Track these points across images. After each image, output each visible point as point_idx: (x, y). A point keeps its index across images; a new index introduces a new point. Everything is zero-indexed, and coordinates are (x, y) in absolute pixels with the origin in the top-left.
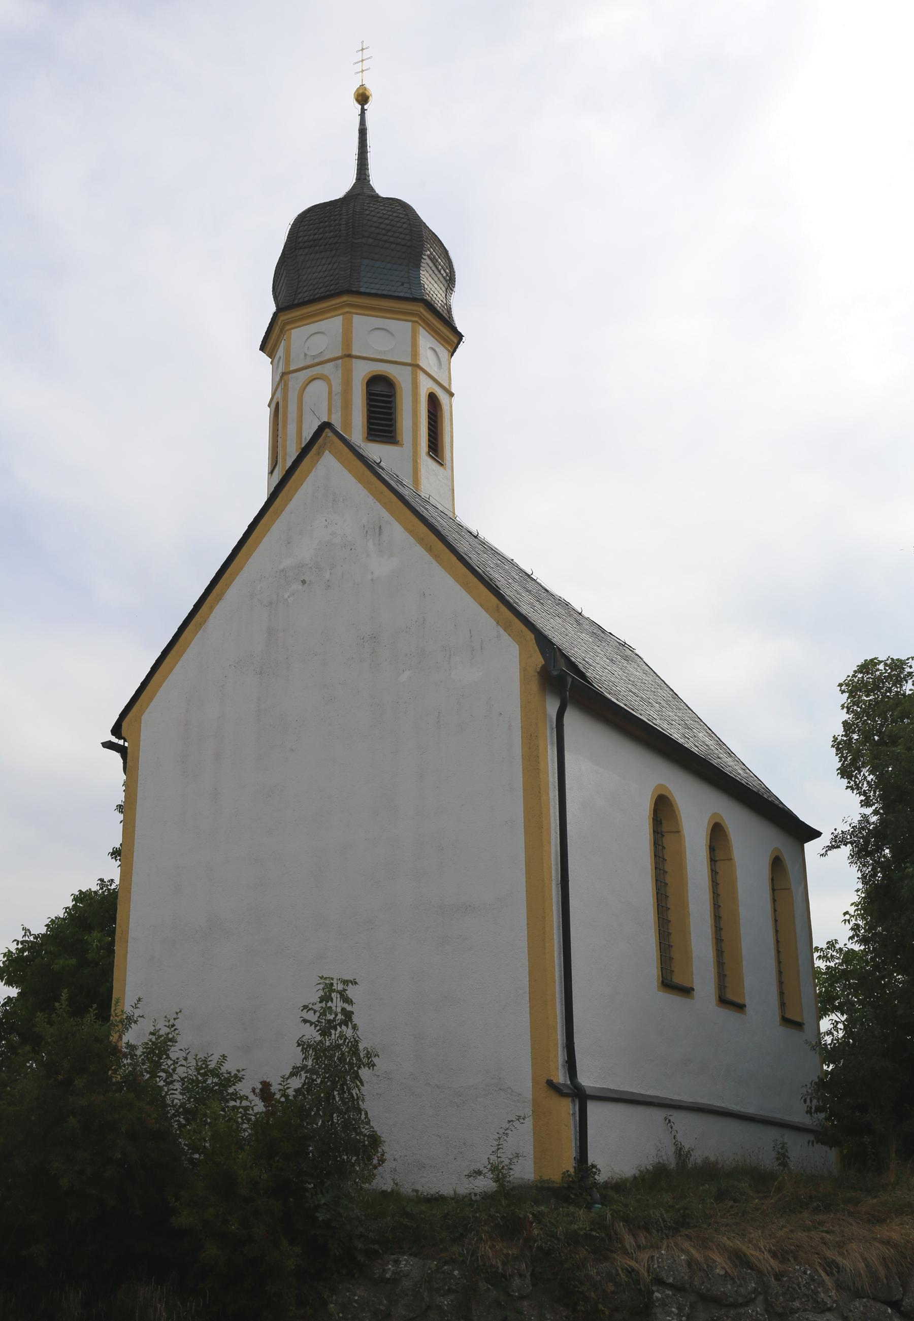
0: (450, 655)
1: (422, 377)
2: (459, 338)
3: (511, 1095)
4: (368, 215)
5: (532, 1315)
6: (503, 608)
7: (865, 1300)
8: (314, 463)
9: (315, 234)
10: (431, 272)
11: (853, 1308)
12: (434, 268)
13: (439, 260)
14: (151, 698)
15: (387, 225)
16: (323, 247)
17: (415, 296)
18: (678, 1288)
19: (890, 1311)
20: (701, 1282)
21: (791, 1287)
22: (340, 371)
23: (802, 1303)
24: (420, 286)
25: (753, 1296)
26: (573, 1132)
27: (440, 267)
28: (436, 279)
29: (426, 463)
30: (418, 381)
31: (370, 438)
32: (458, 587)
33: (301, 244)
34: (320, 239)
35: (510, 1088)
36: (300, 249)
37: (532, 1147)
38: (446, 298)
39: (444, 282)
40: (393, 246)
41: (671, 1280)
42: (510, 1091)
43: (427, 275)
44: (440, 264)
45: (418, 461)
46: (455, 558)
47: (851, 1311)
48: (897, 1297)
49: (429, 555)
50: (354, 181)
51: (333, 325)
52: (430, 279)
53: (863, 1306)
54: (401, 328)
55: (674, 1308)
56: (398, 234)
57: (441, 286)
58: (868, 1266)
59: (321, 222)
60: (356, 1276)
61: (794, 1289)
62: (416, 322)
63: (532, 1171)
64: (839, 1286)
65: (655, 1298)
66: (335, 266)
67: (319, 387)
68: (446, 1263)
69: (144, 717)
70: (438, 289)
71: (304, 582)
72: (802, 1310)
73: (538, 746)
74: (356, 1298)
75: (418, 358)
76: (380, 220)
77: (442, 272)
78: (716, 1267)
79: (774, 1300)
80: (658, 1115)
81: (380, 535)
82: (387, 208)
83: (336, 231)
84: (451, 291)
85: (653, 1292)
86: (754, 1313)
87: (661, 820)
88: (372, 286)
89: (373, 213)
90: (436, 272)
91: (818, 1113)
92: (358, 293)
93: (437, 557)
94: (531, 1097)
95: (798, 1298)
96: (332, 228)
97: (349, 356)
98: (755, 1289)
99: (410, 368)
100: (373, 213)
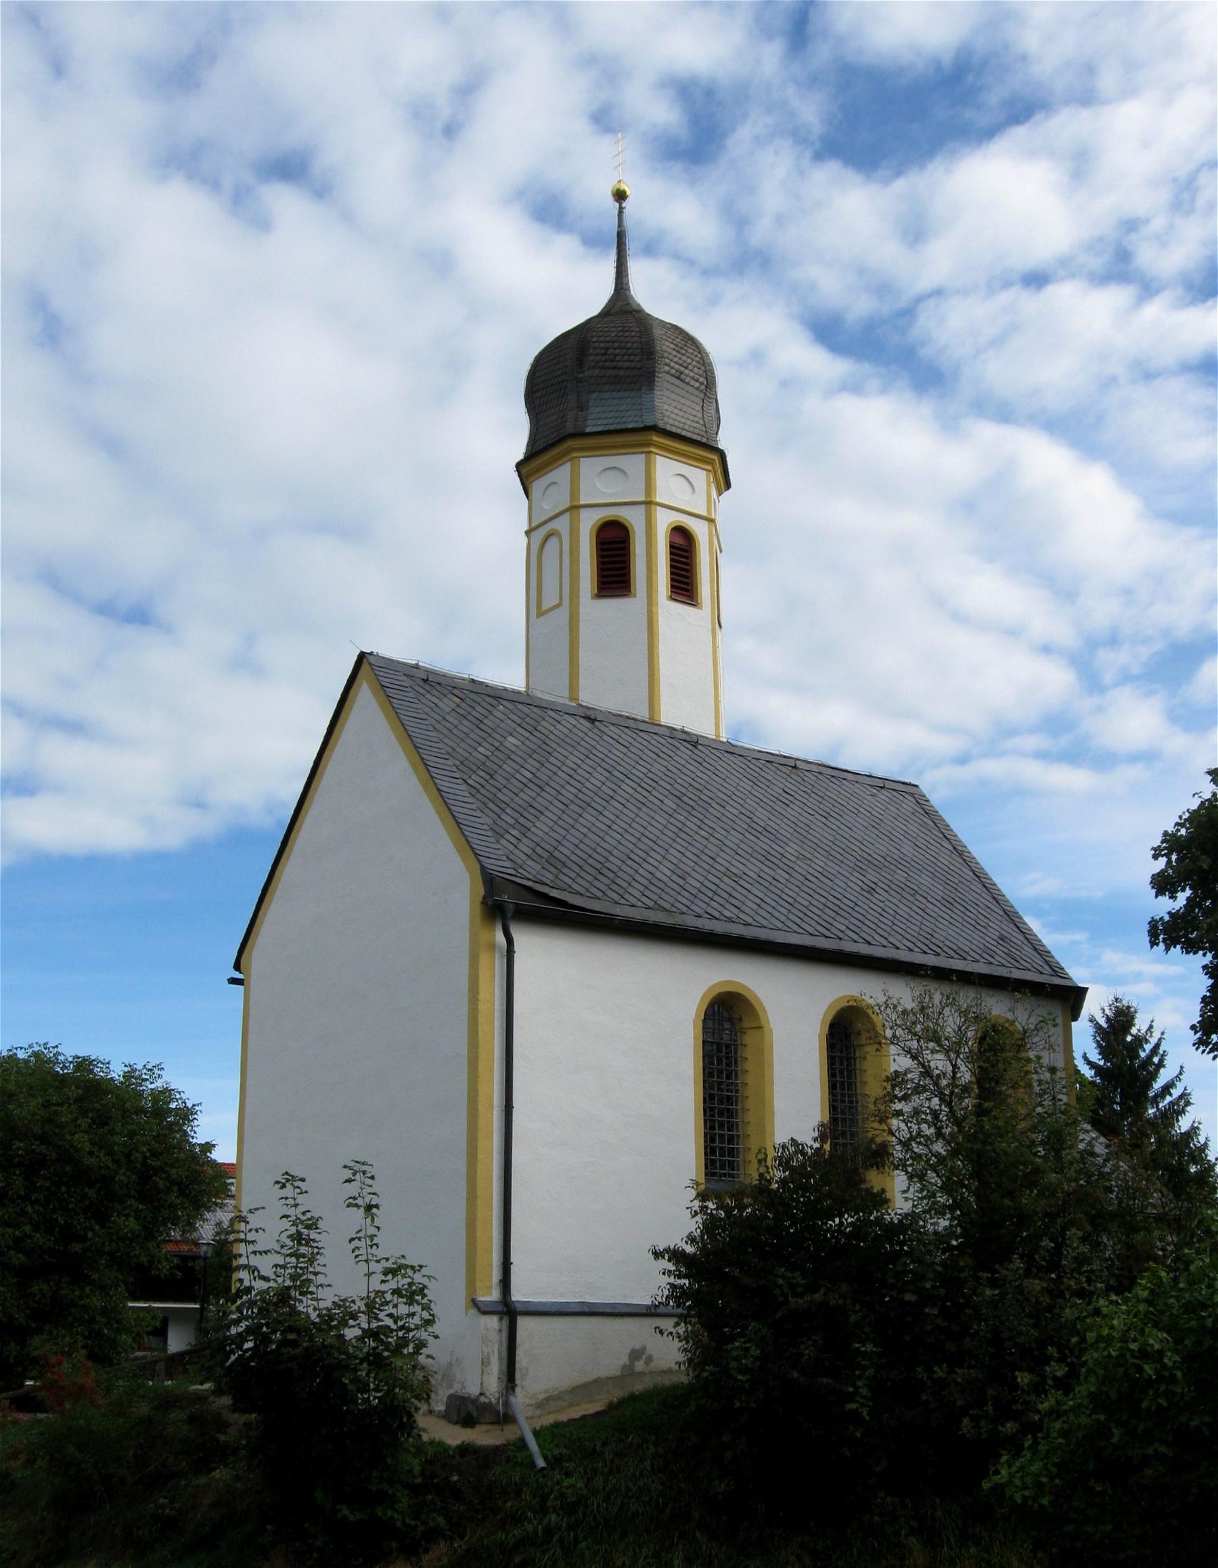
28: (683, 393)
29: (670, 612)
39: (697, 393)
45: (654, 610)
50: (612, 292)
51: (561, 474)
54: (633, 463)
57: (693, 398)
67: (553, 543)
69: (253, 954)
70: (688, 403)
77: (692, 383)
91: (396, 1296)
92: (584, 435)
99: (643, 507)
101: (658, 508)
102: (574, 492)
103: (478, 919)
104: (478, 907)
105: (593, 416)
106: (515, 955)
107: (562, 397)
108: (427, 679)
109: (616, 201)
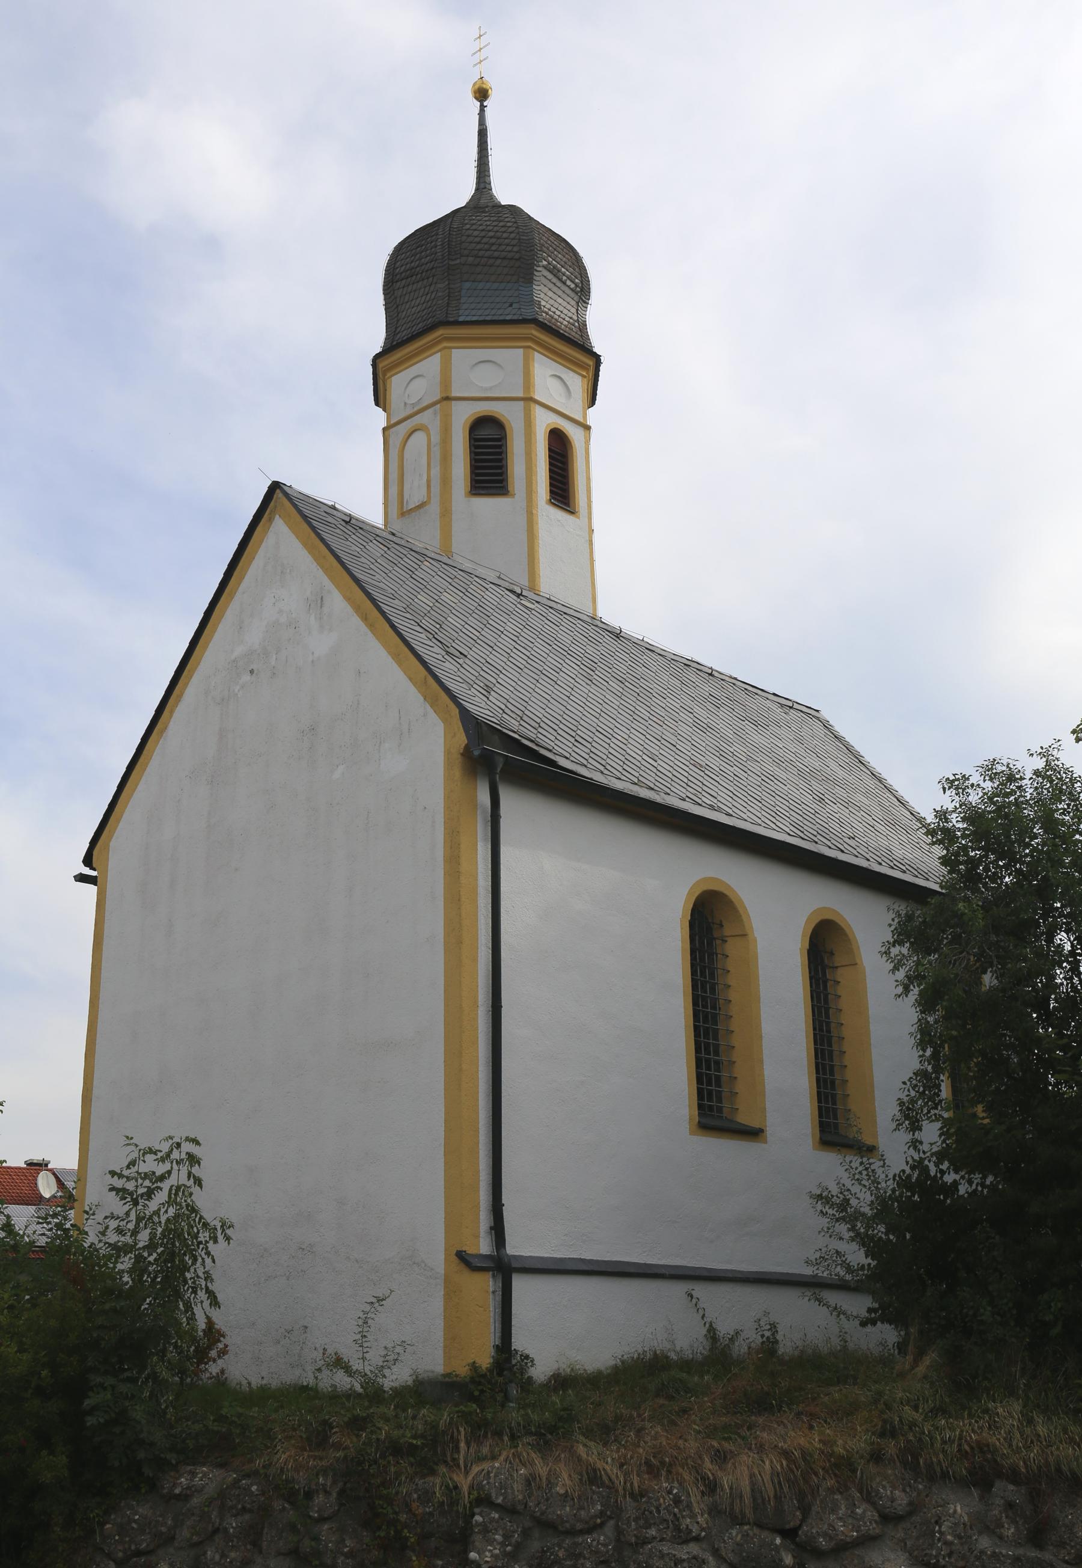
0: (380, 742)
1: (538, 411)
2: (595, 360)
3: (425, 1270)
4: (468, 229)
5: (330, 1542)
6: (431, 681)
7: (746, 1527)
8: (266, 531)
9: (412, 262)
10: (551, 286)
11: (728, 1537)
12: (555, 280)
13: (563, 270)
14: (118, 821)
15: (491, 237)
16: (419, 276)
17: (525, 317)
18: (510, 1510)
19: (778, 1541)
20: (536, 1503)
21: (648, 1511)
22: (438, 418)
23: (659, 1530)
24: (532, 303)
25: (599, 1521)
26: (492, 1314)
27: (564, 278)
28: (560, 293)
29: (548, 515)
30: (532, 417)
31: (474, 492)
32: (390, 660)
33: (398, 277)
34: (418, 266)
35: (424, 1262)
36: (397, 282)
37: (442, 1333)
38: (577, 313)
39: (572, 294)
40: (498, 262)
41: (500, 1500)
42: (423, 1265)
43: (545, 290)
44: (564, 274)
45: (534, 512)
46: (388, 625)
47: (724, 1541)
48: (792, 1525)
49: (364, 626)
50: (473, 192)
51: (430, 365)
52: (550, 294)
53: (743, 1535)
54: (510, 357)
55: (499, 1535)
56: (504, 247)
57: (569, 300)
58: (753, 1484)
59: (418, 247)
60: (143, 1491)
61: (651, 1513)
62: (529, 347)
63: (441, 1362)
64: (714, 1511)
65: (474, 1522)
66: (433, 296)
67: (419, 438)
68: (247, 1476)
69: (112, 844)
70: (565, 304)
71: (252, 672)
72: (658, 1540)
73: (459, 844)
74: (137, 1517)
75: (532, 390)
76: (483, 234)
77: (569, 283)
78: (557, 1485)
79: (625, 1526)
80: (678, 1289)
81: (321, 607)
82: (492, 219)
83: (432, 254)
84: (584, 305)
85: (473, 1515)
86: (595, 1543)
87: (721, 921)
88: (474, 312)
89: (474, 227)
90: (559, 284)
93: (371, 626)
94: (443, 1272)
95: (655, 1524)
96: (428, 252)
97: (447, 399)
98: (602, 1513)
99: (522, 403)
100: (474, 227)
101: (537, 407)
102: (446, 380)
103: (457, 773)
104: (458, 759)
105: (465, 306)
106: (501, 820)
107: (430, 285)
108: (349, 522)
109: (476, 98)
